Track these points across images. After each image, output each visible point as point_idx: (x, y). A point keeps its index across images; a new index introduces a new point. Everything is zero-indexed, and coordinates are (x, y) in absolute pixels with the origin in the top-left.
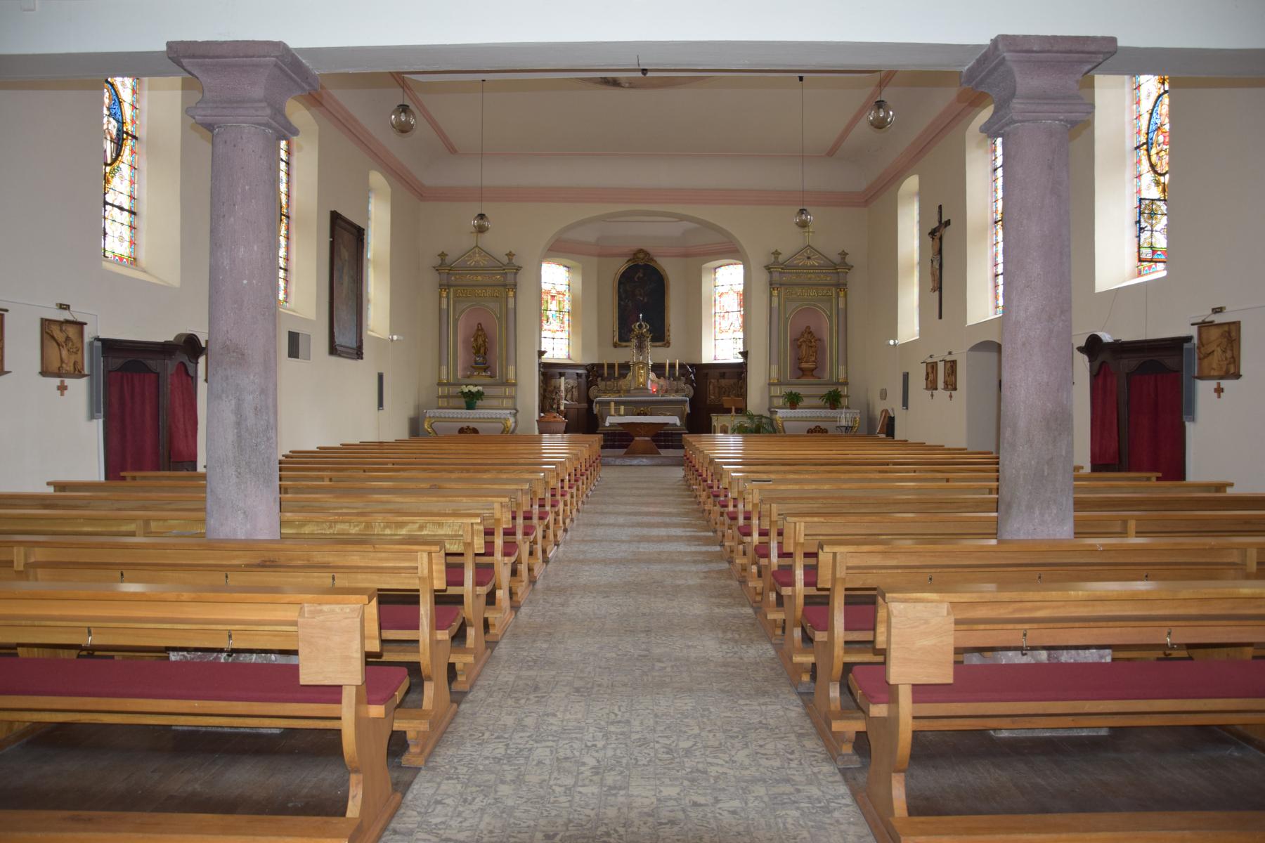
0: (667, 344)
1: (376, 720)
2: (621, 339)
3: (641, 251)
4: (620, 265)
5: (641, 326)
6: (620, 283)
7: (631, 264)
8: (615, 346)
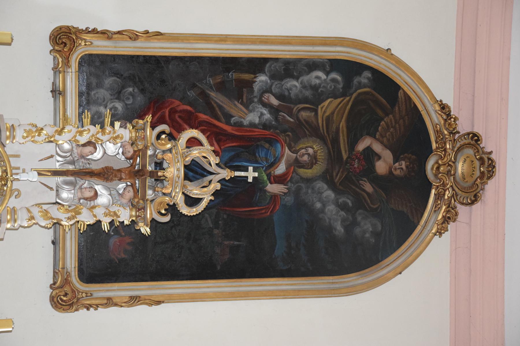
0: (64, 299)
1: (274, 197)
2: (96, 66)
3: (487, 167)
4: (432, 70)
5: (187, 169)
6: (349, 69)
7: (432, 119)
8: (63, 39)
